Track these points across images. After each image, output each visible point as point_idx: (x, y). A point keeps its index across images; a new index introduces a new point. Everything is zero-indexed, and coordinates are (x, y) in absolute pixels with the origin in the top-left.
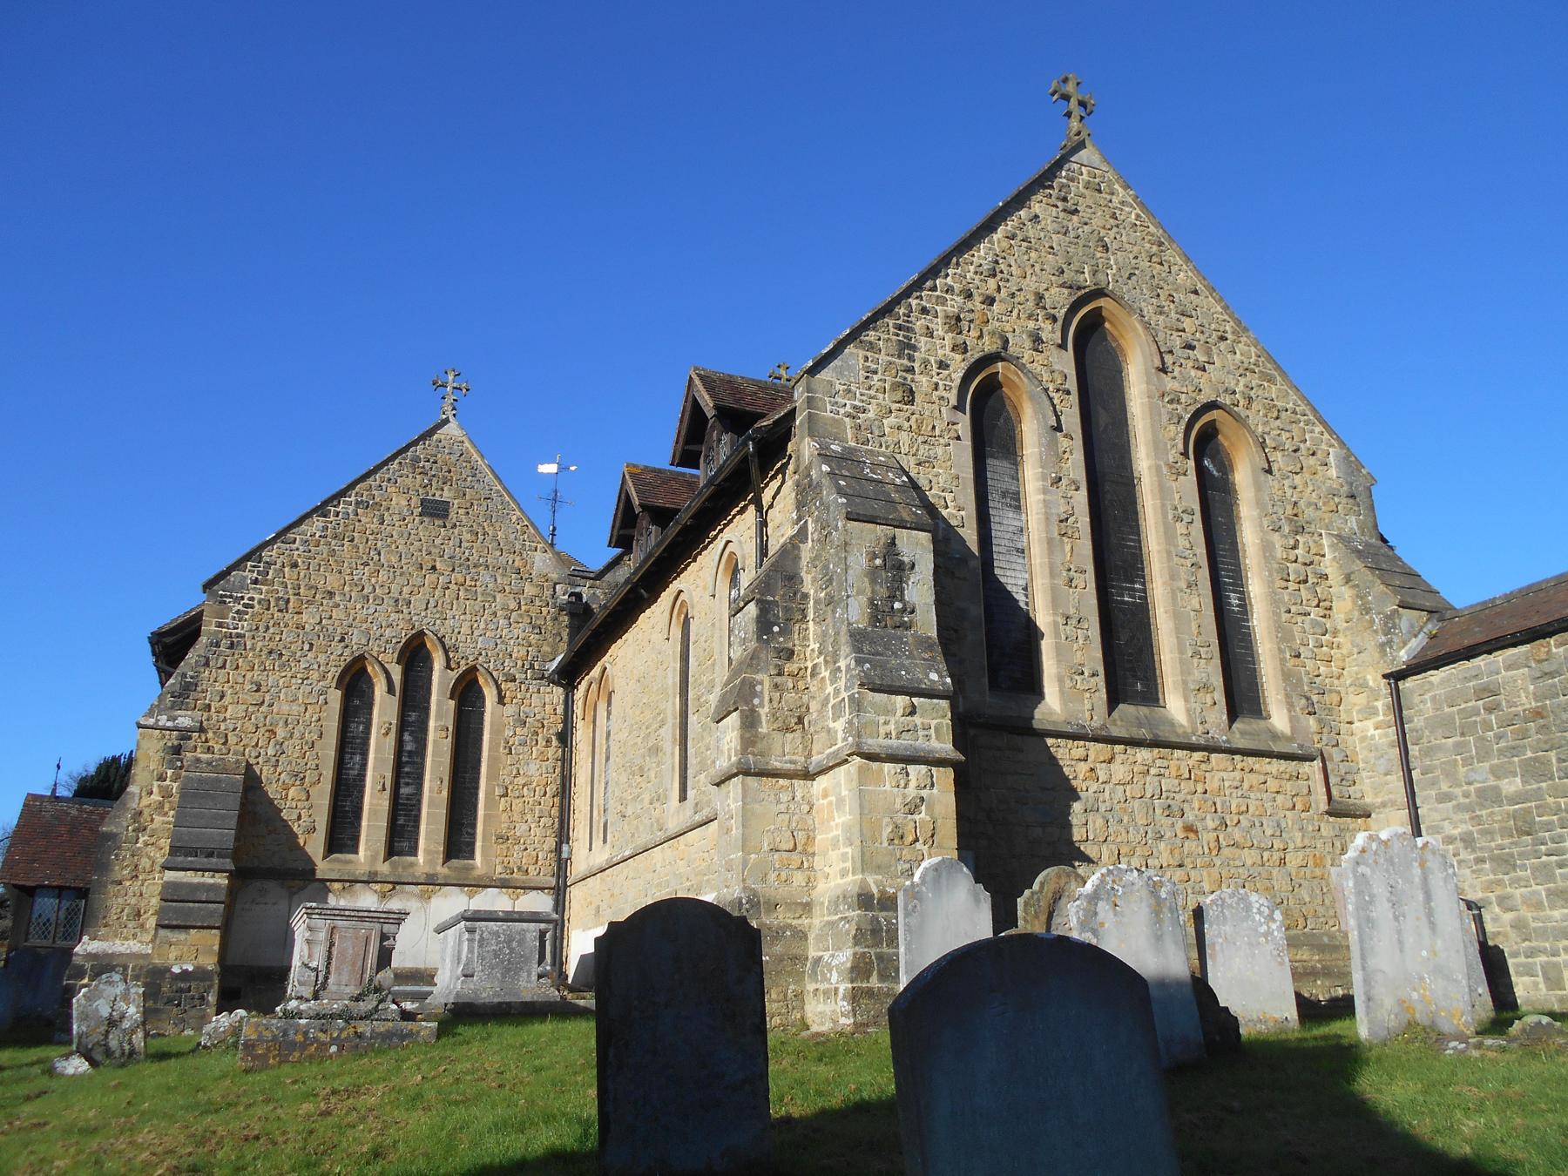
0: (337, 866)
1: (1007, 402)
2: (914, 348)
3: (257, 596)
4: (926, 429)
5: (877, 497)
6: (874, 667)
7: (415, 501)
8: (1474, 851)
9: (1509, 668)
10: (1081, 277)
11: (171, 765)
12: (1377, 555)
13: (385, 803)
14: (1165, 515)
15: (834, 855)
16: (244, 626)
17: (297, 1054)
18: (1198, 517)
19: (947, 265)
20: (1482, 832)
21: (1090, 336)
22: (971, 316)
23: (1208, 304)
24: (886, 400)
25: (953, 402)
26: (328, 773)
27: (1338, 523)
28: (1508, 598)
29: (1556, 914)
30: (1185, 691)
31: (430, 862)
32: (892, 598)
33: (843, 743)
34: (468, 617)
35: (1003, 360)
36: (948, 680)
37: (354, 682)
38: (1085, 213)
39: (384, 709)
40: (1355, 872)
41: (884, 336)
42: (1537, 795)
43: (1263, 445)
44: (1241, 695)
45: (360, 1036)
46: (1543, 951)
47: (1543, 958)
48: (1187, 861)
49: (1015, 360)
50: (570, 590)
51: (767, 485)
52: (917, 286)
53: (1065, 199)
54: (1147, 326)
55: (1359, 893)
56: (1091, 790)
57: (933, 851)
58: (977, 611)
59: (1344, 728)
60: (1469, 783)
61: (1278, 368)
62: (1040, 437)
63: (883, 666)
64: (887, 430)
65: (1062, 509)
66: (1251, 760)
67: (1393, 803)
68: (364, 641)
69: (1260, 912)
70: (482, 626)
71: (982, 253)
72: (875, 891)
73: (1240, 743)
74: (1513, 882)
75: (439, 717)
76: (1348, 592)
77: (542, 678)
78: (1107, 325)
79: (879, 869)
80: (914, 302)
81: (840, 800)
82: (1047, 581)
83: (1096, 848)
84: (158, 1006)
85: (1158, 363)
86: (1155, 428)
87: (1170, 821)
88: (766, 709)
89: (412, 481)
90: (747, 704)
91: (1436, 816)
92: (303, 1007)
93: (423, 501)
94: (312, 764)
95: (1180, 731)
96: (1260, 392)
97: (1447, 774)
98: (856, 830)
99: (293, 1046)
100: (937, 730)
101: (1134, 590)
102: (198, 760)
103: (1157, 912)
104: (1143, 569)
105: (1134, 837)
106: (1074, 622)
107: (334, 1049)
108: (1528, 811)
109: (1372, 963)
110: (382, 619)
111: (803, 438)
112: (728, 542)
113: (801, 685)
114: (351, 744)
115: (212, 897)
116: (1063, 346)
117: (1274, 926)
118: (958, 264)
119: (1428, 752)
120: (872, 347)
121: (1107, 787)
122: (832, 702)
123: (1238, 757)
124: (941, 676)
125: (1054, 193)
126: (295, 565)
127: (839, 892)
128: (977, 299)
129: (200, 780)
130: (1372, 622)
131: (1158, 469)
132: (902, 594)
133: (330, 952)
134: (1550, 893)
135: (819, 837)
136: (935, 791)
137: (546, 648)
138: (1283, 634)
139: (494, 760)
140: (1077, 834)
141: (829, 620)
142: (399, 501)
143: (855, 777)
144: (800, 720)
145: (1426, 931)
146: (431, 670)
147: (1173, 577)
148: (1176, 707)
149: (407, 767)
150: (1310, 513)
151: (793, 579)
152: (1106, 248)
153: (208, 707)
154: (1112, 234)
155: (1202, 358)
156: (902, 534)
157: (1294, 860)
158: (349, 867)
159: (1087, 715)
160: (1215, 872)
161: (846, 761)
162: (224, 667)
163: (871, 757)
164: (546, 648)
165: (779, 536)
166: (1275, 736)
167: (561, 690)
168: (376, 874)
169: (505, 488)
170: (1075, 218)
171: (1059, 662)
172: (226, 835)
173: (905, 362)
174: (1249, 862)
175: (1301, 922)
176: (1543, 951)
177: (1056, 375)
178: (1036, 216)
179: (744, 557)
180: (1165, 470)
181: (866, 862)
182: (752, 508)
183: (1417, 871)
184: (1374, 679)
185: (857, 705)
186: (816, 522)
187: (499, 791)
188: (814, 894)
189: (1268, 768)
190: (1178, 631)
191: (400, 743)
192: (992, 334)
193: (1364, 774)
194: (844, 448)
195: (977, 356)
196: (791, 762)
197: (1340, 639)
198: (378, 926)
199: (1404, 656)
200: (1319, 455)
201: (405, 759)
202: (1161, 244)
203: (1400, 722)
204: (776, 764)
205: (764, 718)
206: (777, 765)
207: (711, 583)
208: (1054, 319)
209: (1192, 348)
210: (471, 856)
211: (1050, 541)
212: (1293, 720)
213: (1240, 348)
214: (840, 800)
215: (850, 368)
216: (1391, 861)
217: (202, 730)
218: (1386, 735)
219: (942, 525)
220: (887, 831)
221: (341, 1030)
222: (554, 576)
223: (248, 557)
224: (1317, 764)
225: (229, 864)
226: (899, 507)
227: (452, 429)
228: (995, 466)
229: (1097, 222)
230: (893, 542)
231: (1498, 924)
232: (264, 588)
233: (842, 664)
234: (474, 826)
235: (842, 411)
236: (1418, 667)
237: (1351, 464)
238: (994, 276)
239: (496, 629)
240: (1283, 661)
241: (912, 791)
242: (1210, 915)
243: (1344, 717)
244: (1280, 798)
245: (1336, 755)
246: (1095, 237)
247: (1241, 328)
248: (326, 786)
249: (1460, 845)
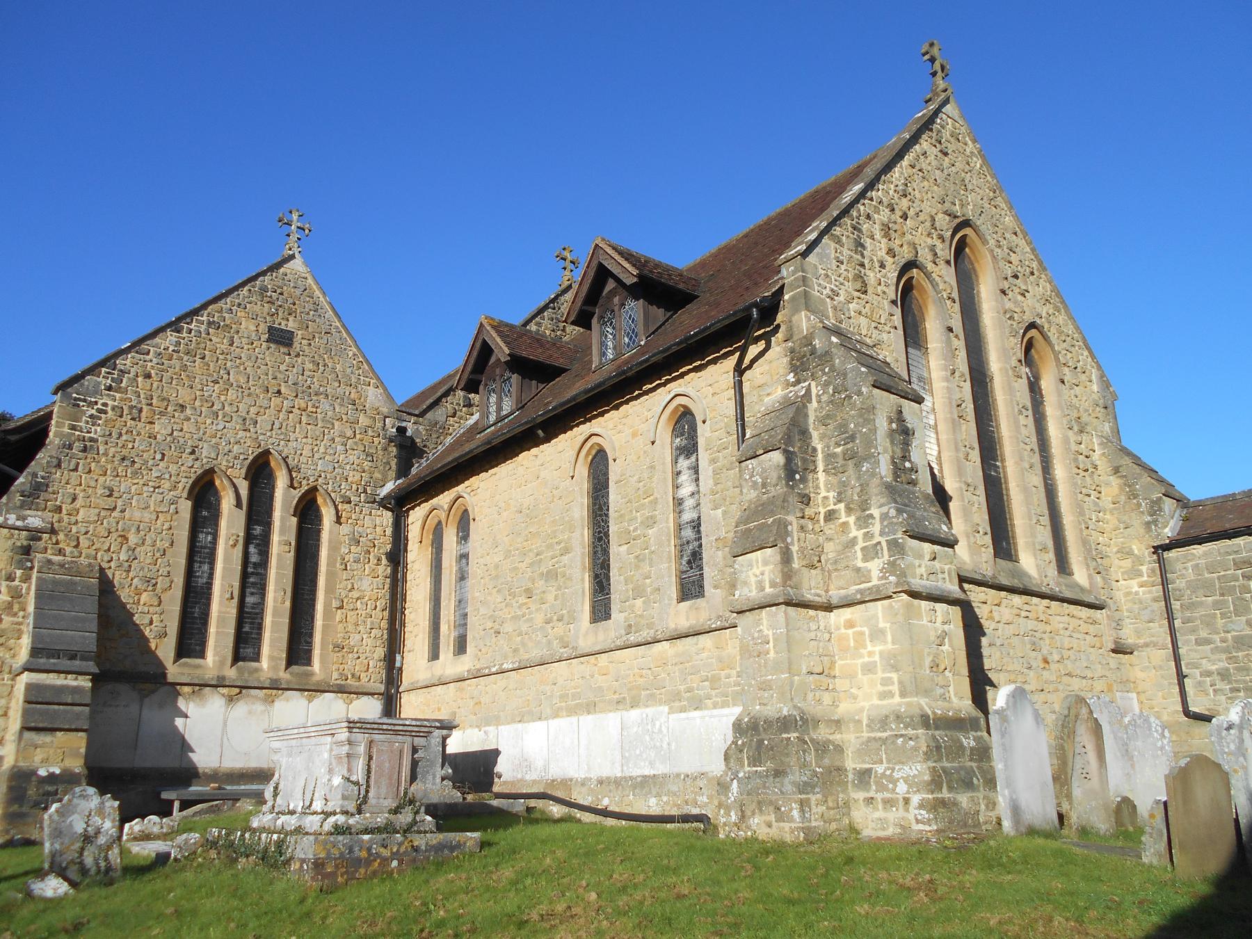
0: (186, 670)
2: (863, 246)
3: (110, 403)
7: (263, 328)
8: (1230, 682)
11: (20, 565)
13: (233, 612)
16: (97, 431)
17: (362, 871)
20: (1237, 669)
24: (849, 286)
26: (179, 581)
31: (274, 668)
34: (309, 441)
37: (203, 493)
39: (231, 521)
45: (416, 849)
50: (398, 424)
61: (1063, 302)
65: (958, 396)
68: (213, 455)
70: (322, 450)
72: (930, 713)
75: (282, 532)
76: (1115, 481)
77: (373, 502)
78: (967, 250)
84: (24, 809)
92: (351, 821)
93: (270, 328)
94: (164, 571)
99: (358, 862)
102: (49, 562)
107: (395, 863)
110: (230, 435)
114: (199, 555)
115: (78, 699)
117: (1165, 742)
119: (1192, 606)
126: (148, 376)
129: (55, 582)
130: (1139, 505)
133: (369, 766)
137: (377, 475)
139: (331, 575)
142: (248, 326)
146: (273, 488)
149: (252, 576)
153: (59, 509)
158: (198, 672)
161: (890, 597)
162: (76, 470)
163: (914, 595)
164: (377, 475)
167: (390, 514)
168: (224, 678)
169: (343, 326)
172: (87, 638)
184: (1141, 548)
185: (894, 545)
187: (335, 604)
191: (246, 554)
198: (409, 739)
201: (250, 570)
204: (809, 597)
207: (653, 430)
210: (309, 662)
217: (53, 531)
220: (928, 661)
221: (400, 844)
222: (385, 410)
223: (102, 363)
225: (92, 667)
227: (297, 265)
232: (118, 395)
233: (875, 512)
234: (311, 635)
239: (335, 454)
248: (177, 592)
249: (1216, 678)
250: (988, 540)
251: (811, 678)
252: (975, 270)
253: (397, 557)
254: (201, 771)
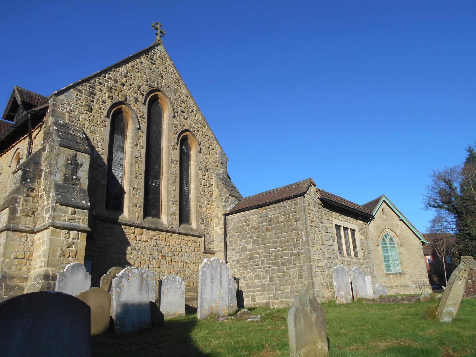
1: (124, 118)
2: (95, 94)
4: (95, 121)
5: (70, 139)
6: (62, 197)
9: (253, 215)
10: (153, 84)
12: (226, 181)
14: (169, 161)
15: (38, 261)
18: (178, 163)
19: (111, 70)
21: (154, 103)
22: (116, 88)
23: (190, 101)
24: (82, 109)
25: (106, 114)
27: (217, 170)
28: (255, 196)
29: (256, 281)
30: (167, 215)
32: (73, 174)
33: (47, 221)
35: (124, 104)
36: (89, 204)
38: (157, 65)
40: (202, 270)
41: (85, 88)
42: (255, 249)
43: (200, 145)
44: (184, 217)
46: (251, 291)
47: (252, 293)
48: (161, 266)
49: (129, 105)
51: (35, 130)
52: (99, 75)
53: (152, 59)
54: (171, 103)
55: (203, 276)
56: (134, 243)
57: (75, 260)
58: (104, 183)
59: (211, 228)
60: (240, 246)
61: (207, 123)
62: (133, 130)
63: (66, 197)
64: (81, 119)
65: (137, 154)
66: (184, 236)
67: (221, 250)
69: (178, 282)
71: (123, 69)
72: (51, 273)
74: (247, 272)
76: (217, 190)
79: (53, 266)
80: (97, 80)
81: (44, 242)
82: (129, 176)
83: (133, 261)
85: (173, 115)
86: (169, 134)
87: (158, 253)
88: (20, 208)
90: (13, 205)
91: (231, 254)
95: (164, 226)
96: (201, 129)
97: (235, 243)
98: (47, 252)
100: (82, 220)
101: (157, 182)
103: (141, 282)
104: (160, 176)
105: (146, 258)
106: (136, 190)
108: (253, 253)
109: (203, 296)
111: (49, 117)
112: (18, 148)
113: (36, 201)
116: (144, 104)
117: (182, 286)
118: (114, 71)
119: (231, 237)
120: (80, 91)
121: (140, 242)
122: (46, 207)
123: (180, 235)
124: (86, 202)
125: (149, 56)
127: (38, 274)
128: (119, 83)
131: (169, 146)
132: (77, 174)
134: (255, 276)
135: (34, 254)
136: (79, 240)
138: (198, 200)
140: (128, 257)
141: (49, 179)
143: (50, 234)
144: (33, 213)
145: (219, 287)
147: (169, 180)
148: (164, 219)
150: (210, 166)
151: (38, 164)
152: (162, 77)
154: (165, 73)
155: (186, 116)
156: (80, 155)
159: (136, 219)
160: (169, 269)
161: (47, 228)
165: (35, 149)
166: (192, 230)
170: (154, 66)
171: (129, 202)
173: (91, 98)
174: (180, 267)
175: (192, 284)
176: (251, 291)
177: (141, 112)
178: (142, 62)
179: (23, 154)
180: (170, 147)
181: (49, 264)
182: (28, 138)
183: (219, 270)
184: (221, 215)
185: (54, 209)
186: (49, 145)
188: (30, 274)
189: (189, 239)
190: (168, 196)
192: (122, 95)
193: (215, 242)
194: (64, 123)
195: (116, 101)
196: (28, 227)
197: (214, 203)
199: (228, 209)
200: (215, 150)
202: (179, 80)
203: (226, 228)
205: (19, 211)
206: (22, 228)
207: (10, 162)
208: (143, 95)
209: (184, 112)
211: (132, 164)
212: (198, 225)
213: (197, 115)
214: (44, 242)
215: (71, 97)
216: (212, 267)
218: (222, 231)
219: (95, 153)
220: (59, 253)
224: (203, 238)
226: (80, 145)
228: (117, 138)
229: (160, 69)
230: (76, 156)
231: (242, 284)
233: (51, 195)
235: (65, 110)
236: (231, 213)
237: (223, 154)
238: (126, 77)
240: (197, 208)
241: (70, 240)
242: (164, 282)
243: (212, 225)
244: (191, 248)
245: (208, 236)
246: (159, 73)
247: (198, 110)
249: (236, 262)
250: (142, 209)
251: (17, 260)
252: (163, 109)
253: (339, 237)
254: (166, 318)
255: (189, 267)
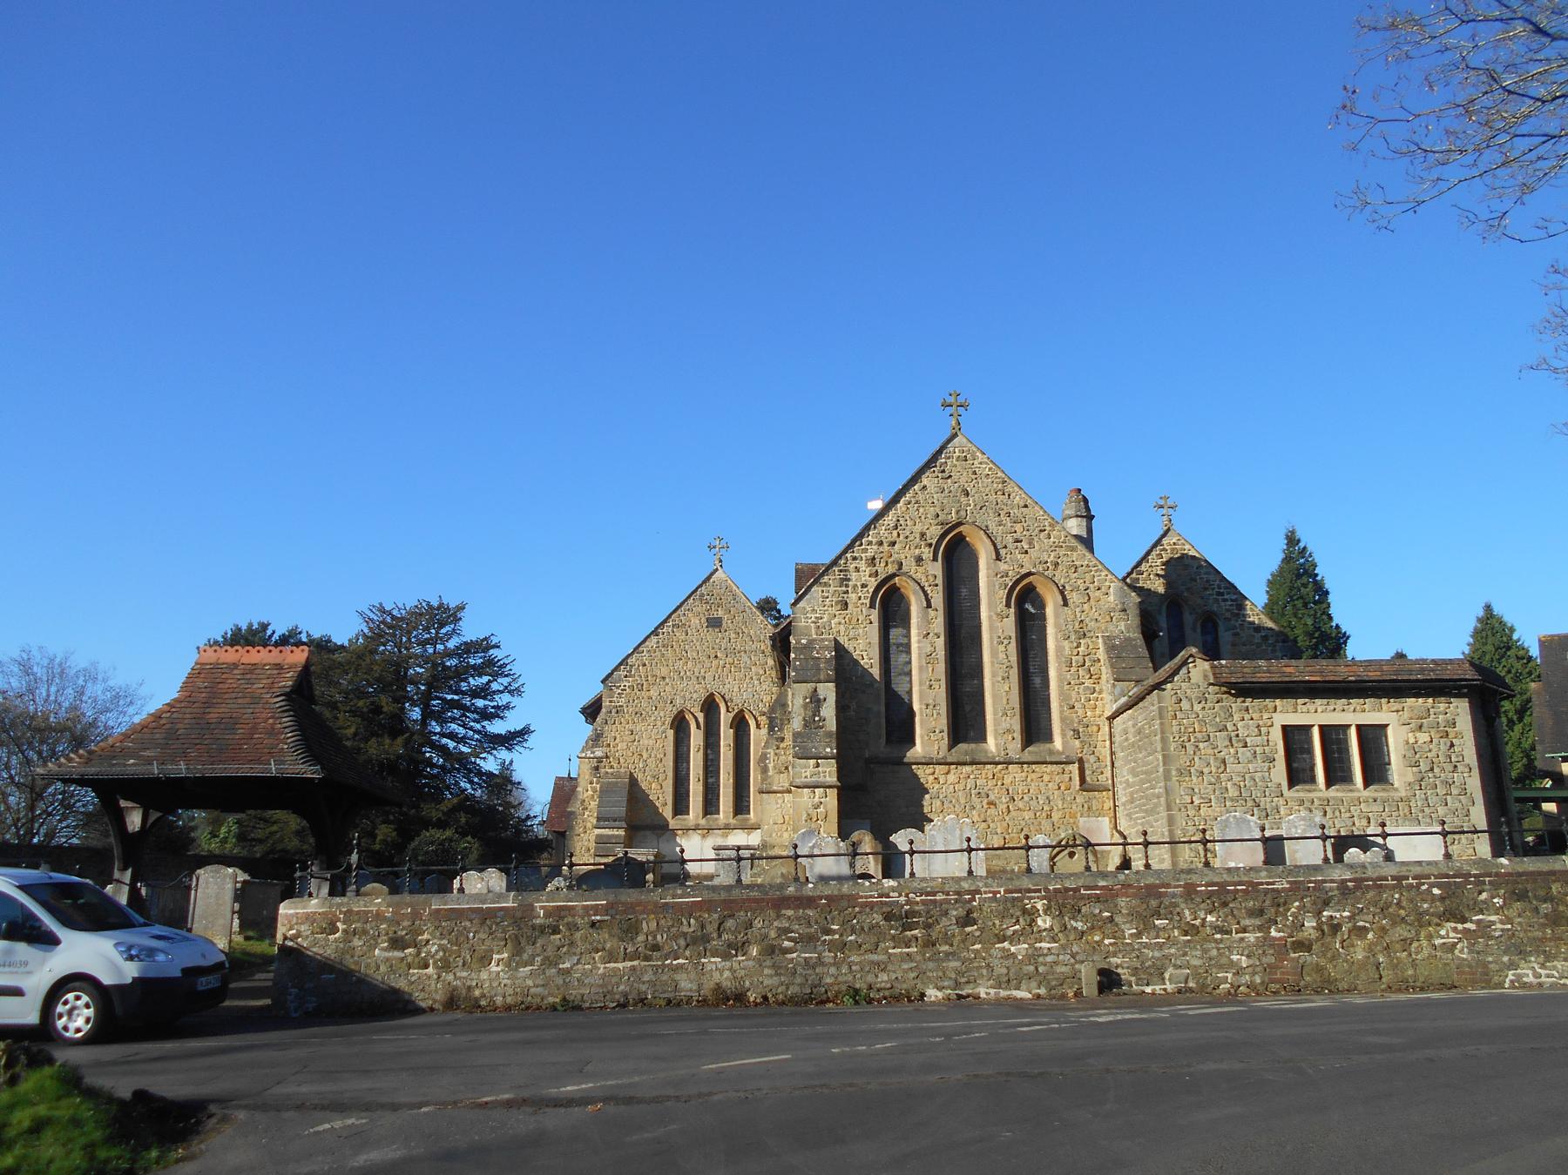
26: (670, 774)
37: (680, 725)
38: (955, 476)
39: (696, 738)
63: (804, 748)
65: (929, 649)
73: (1030, 759)
89: (701, 608)
114: (681, 757)
138: (1064, 697)
142: (695, 621)
148: (991, 743)
149: (711, 767)
157: (1056, 816)
166: (1051, 752)
172: (622, 810)
212: (1064, 744)
224: (1075, 768)
229: (963, 480)
255: (1049, 817)
